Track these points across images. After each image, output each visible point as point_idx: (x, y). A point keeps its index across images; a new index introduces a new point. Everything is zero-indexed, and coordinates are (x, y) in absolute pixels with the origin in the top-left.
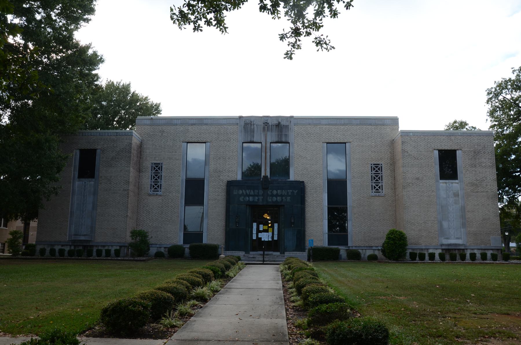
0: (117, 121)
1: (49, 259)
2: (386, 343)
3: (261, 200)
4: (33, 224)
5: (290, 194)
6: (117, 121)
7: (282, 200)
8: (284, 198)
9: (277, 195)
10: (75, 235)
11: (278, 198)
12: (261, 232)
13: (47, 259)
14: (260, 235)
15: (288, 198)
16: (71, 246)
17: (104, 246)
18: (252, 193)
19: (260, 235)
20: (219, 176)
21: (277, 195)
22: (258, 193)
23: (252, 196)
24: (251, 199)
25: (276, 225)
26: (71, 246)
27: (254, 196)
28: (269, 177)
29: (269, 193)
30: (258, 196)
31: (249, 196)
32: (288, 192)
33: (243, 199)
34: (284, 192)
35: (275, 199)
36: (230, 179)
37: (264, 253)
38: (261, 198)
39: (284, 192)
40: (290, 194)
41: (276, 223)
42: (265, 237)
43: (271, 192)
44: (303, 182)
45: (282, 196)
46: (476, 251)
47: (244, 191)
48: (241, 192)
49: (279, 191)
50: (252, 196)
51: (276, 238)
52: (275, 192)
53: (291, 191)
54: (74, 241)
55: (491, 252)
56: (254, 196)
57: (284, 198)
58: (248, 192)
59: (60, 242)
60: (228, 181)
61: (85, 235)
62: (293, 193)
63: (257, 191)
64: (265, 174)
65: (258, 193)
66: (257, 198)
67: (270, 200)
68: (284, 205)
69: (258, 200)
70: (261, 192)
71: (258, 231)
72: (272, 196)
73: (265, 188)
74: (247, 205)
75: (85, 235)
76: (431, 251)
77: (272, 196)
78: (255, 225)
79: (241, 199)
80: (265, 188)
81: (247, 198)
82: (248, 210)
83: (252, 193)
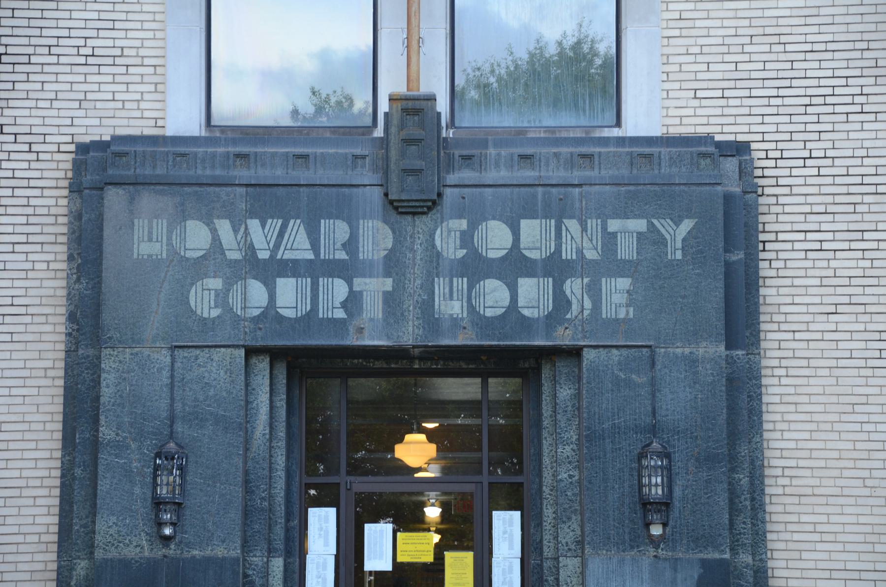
0: (437, 365)
2: (761, 582)
3: (373, 309)
5: (626, 250)
6: (437, 365)
7: (561, 302)
8: (573, 287)
9: (514, 266)
11: (527, 287)
15: (617, 293)
18: (297, 245)
21: (514, 266)
22: (351, 245)
23: (292, 268)
24: (289, 295)
25: (506, 527)
27: (315, 270)
28: (442, 106)
29: (447, 237)
30: (343, 271)
31: (270, 270)
32: (610, 239)
33: (222, 298)
34: (579, 240)
35: (494, 296)
38: (374, 288)
39: (579, 240)
40: (626, 250)
41: (319, 502)
43: (466, 239)
44: (740, 149)
45: (555, 268)
47: (224, 227)
48: (196, 237)
49: (532, 230)
50: (292, 268)
52: (496, 238)
53: (639, 225)
56: (315, 270)
57: (573, 287)
58: (260, 234)
60: (83, 149)
62: (652, 240)
63: (341, 230)
64: (412, 79)
65: (351, 245)
66: (340, 289)
67: (456, 308)
68: (575, 353)
69: (353, 302)
70: (376, 237)
72: (475, 267)
73: (411, 206)
74: (251, 352)
77: (475, 267)
78: (322, 525)
79: (203, 299)
80: (411, 206)
81: (257, 293)
82: (262, 399)
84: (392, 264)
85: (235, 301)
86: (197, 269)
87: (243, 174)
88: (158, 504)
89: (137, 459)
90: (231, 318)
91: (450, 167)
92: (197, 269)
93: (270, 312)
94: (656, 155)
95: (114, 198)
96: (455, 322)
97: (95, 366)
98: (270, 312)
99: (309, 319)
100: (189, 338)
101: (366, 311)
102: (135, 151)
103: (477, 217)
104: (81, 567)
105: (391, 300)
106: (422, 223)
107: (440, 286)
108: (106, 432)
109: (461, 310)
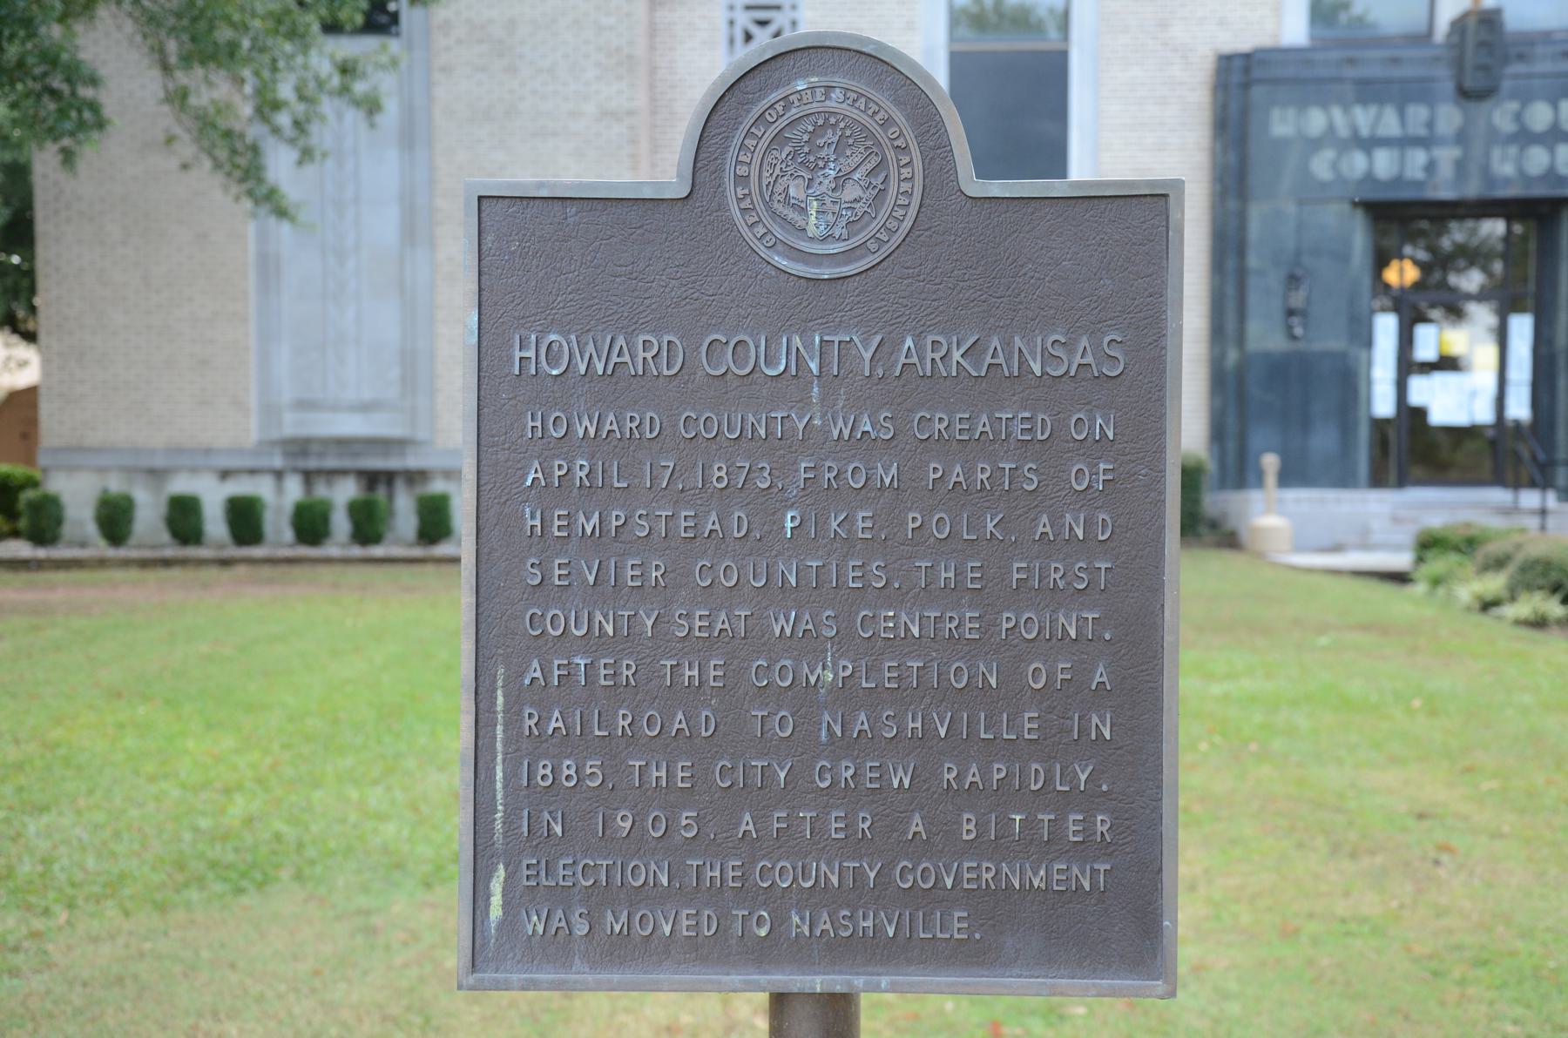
1: (167, 563)
3: (1446, 171)
4: (1383, 404)
10: (303, 405)
12: (1428, 368)
13: (144, 564)
14: (1422, 390)
16: (279, 475)
17: (156, 475)
18: (1390, 124)
19: (1422, 390)
20: (1163, 25)
22: (1430, 124)
24: (1384, 163)
26: (279, 475)
27: (1404, 143)
29: (1502, 116)
30: (1425, 142)
31: (1369, 144)
33: (1335, 166)
36: (1243, 42)
37: (1516, 501)
38: (1447, 156)
42: (1451, 402)
43: (1518, 117)
46: (262, 488)
48: (1316, 121)
51: (1519, 408)
52: (1540, 116)
54: (299, 447)
55: (330, 550)
56: (1404, 143)
58: (1363, 118)
59: (208, 452)
61: (365, 408)
65: (1430, 124)
69: (1431, 167)
70: (1449, 117)
71: (1407, 366)
75: (365, 408)
76: (181, 485)
77: (1524, 137)
79: (1321, 166)
83: (1390, 124)
84: (1461, 138)
85: (1344, 167)
86: (1315, 144)
87: (1350, 72)
88: (1291, 313)
89: (1275, 279)
90: (1340, 179)
91: (1506, 60)
92: (1315, 144)
93: (1369, 178)
94: (442, 549)
95: (1258, 93)
96: (1507, 181)
97: (1242, 217)
98: (1369, 178)
99: (1398, 181)
100: (1312, 193)
101: (1435, 171)
102: (455, 560)
103: (1526, 98)
104: (1232, 356)
105: (1460, 166)
106: (1485, 106)
107: (1496, 153)
108: (1253, 261)
109: (1517, 169)
